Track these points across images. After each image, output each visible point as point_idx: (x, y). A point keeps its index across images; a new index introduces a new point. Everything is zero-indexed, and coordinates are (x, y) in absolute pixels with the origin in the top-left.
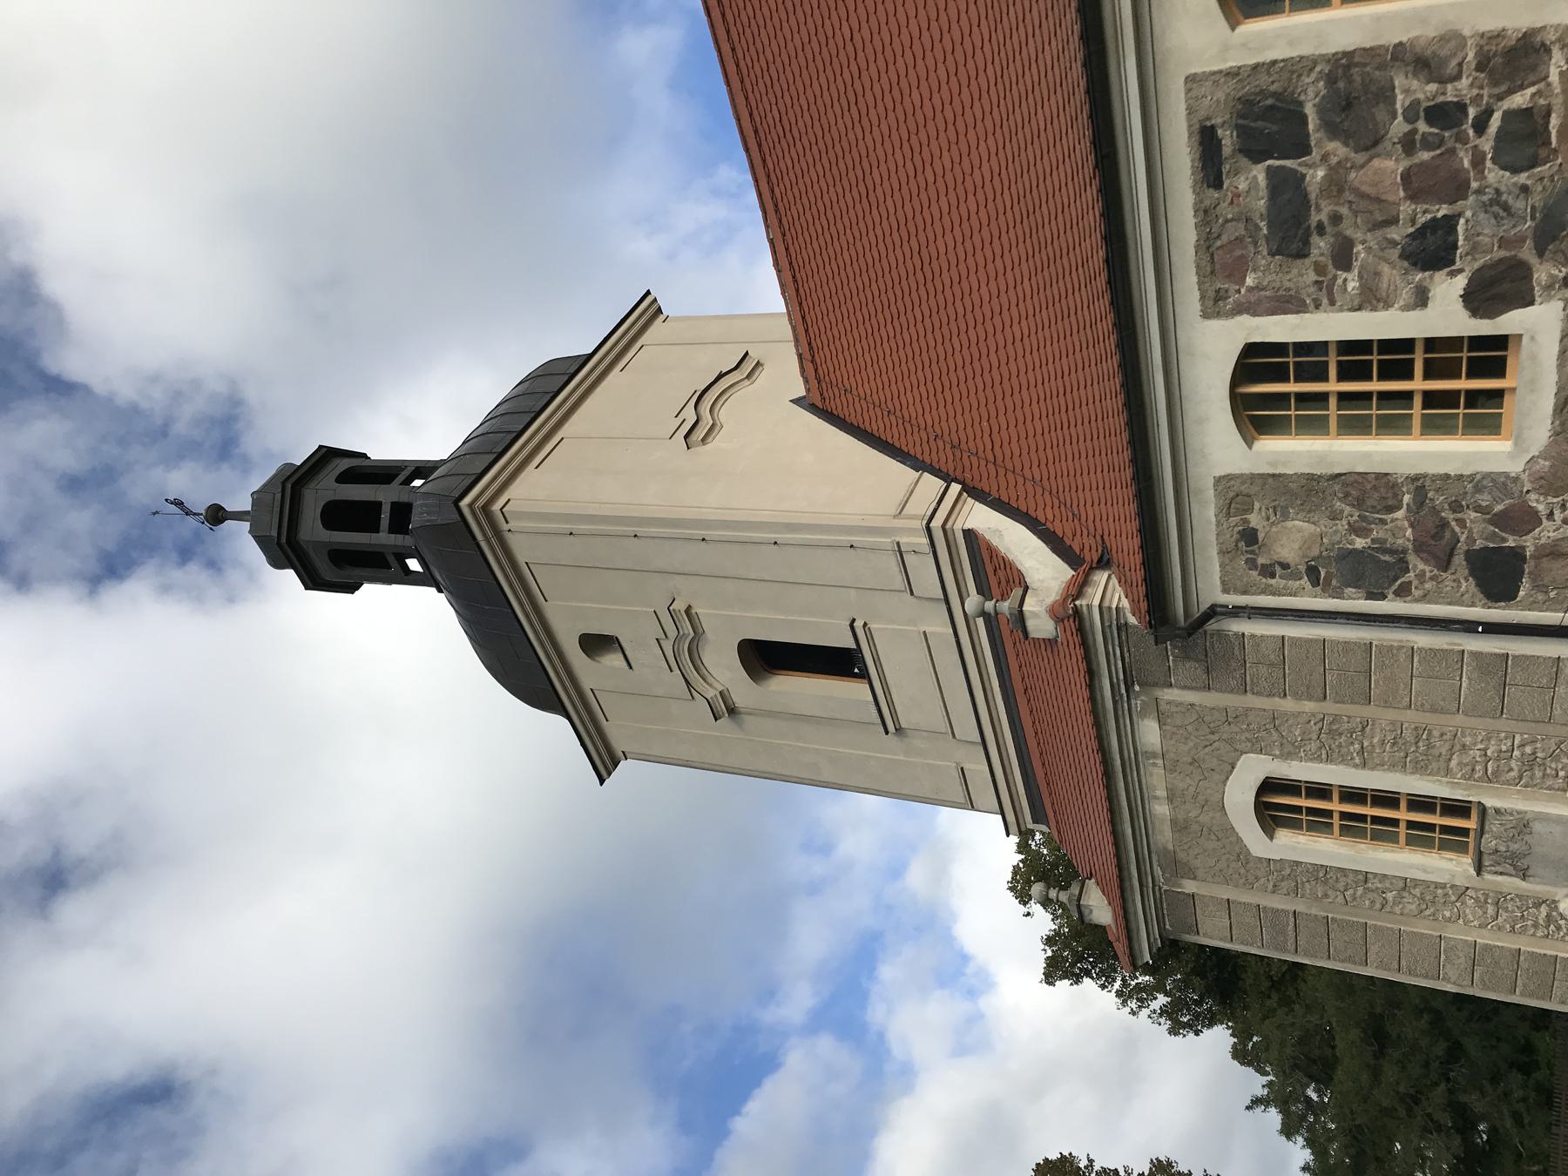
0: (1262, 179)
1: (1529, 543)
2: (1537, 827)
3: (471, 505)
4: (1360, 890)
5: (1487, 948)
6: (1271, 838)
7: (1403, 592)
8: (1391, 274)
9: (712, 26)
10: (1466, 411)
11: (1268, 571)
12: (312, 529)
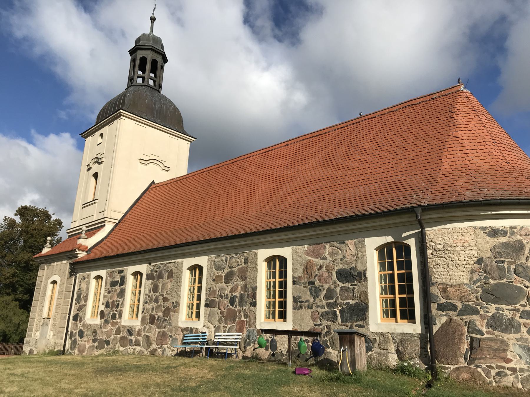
0: (118, 280)
1: (78, 322)
2: (47, 327)
3: (121, 112)
4: (43, 299)
5: (34, 320)
6: (188, 269)
7: (76, 304)
8: (106, 299)
9: (181, 177)
10: (389, 310)
11: (80, 282)
12: (140, 54)
